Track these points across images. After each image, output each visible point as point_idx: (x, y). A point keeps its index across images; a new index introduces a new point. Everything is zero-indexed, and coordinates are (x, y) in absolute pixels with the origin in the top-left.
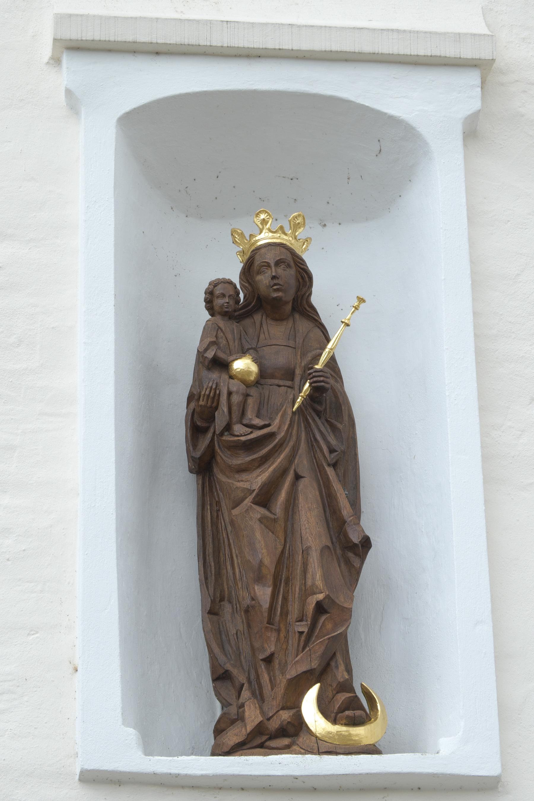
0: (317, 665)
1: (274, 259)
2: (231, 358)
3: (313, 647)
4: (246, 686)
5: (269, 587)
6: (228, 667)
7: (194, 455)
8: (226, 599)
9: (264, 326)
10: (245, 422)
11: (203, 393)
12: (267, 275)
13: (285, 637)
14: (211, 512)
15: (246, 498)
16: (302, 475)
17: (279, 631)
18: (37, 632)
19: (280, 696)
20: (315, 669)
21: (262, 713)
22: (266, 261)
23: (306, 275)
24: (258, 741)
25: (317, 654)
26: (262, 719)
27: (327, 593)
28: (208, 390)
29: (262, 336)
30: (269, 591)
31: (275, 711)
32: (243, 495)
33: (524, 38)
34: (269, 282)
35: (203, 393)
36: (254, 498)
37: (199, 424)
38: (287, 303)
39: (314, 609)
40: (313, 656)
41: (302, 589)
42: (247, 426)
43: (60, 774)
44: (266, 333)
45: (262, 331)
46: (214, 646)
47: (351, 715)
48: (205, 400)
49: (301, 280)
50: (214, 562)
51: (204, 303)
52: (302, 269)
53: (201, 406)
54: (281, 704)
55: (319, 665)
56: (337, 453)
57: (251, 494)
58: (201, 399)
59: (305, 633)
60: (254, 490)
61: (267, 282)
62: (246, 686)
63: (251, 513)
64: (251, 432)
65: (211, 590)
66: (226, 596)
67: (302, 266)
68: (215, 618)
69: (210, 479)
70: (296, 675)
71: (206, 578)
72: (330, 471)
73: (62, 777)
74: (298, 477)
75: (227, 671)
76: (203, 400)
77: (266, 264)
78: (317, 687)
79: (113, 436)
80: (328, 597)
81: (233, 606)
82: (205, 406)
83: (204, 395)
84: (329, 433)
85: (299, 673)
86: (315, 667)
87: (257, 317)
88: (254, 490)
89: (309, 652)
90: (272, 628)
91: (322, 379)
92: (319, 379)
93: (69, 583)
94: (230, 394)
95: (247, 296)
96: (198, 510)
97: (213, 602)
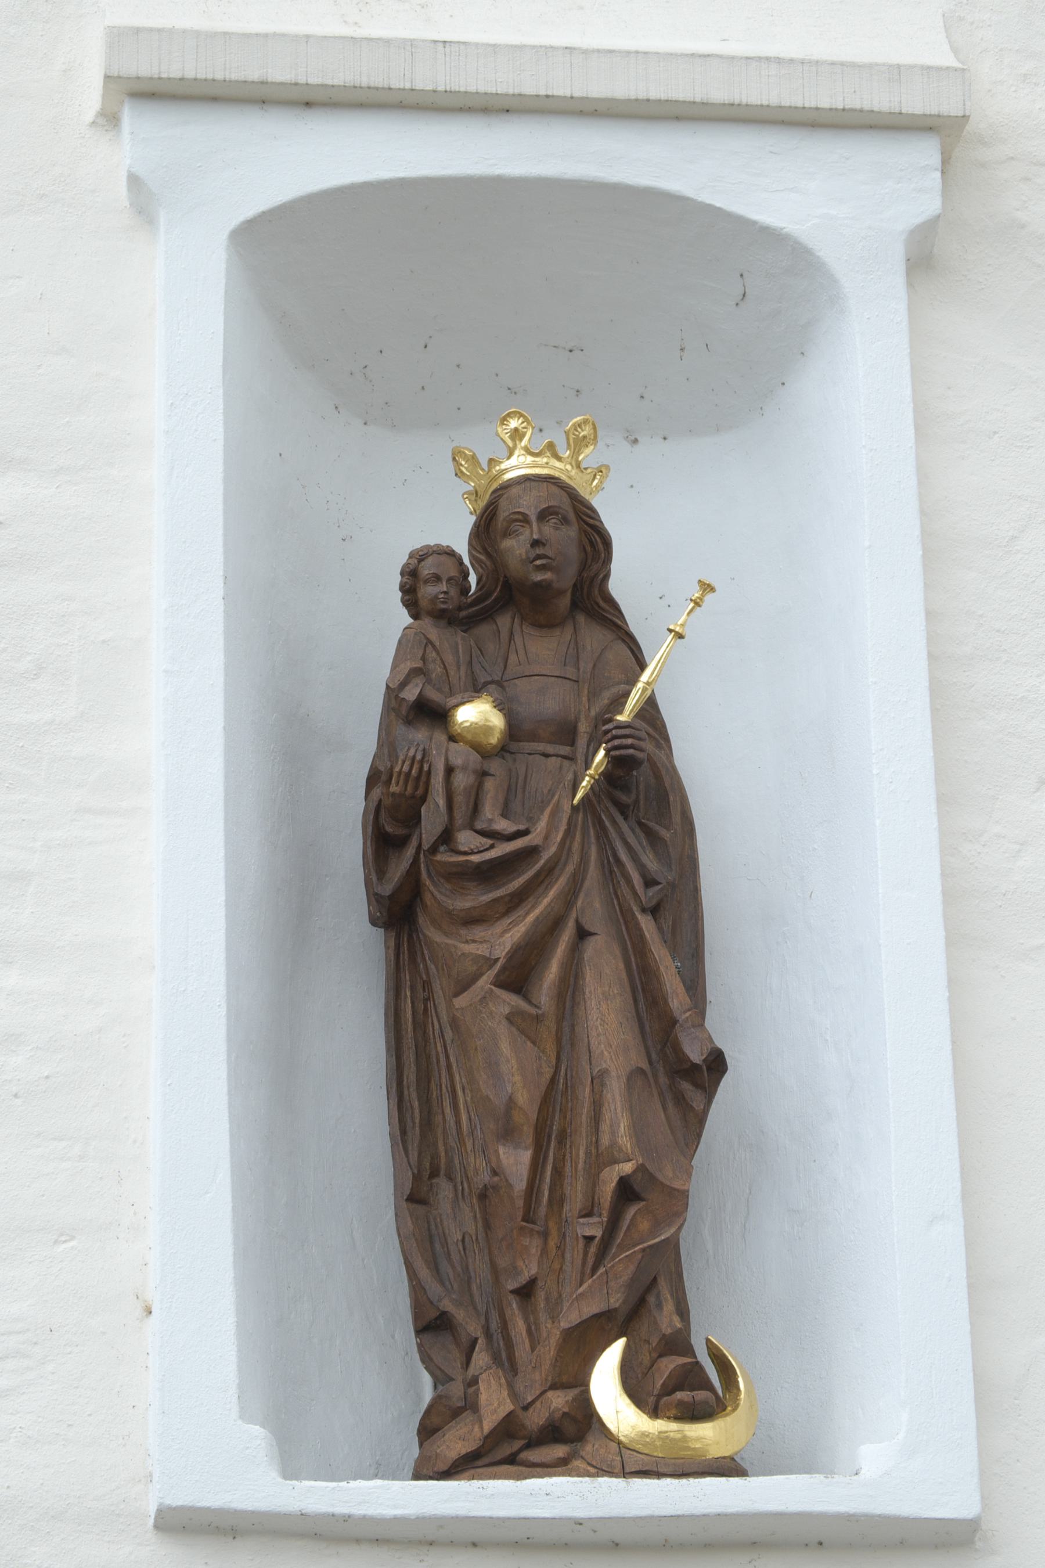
0: (620, 1301)
1: (536, 508)
2: (452, 701)
3: (613, 1266)
4: (481, 1343)
5: (526, 1148)
6: (447, 1305)
7: (379, 890)
8: (442, 1172)
9: (517, 638)
10: (479, 826)
11: (397, 769)
12: (522, 537)
13: (558, 1248)
14: (413, 1003)
15: (482, 974)
16: (592, 930)
17: (545, 1235)
18: (73, 1238)
19: (548, 1362)
20: (615, 1310)
21: (514, 1395)
22: (521, 510)
23: (598, 539)
24: (506, 1450)
25: (621, 1281)
26: (512, 1407)
27: (641, 1161)
28: (408, 763)
29: (513, 658)
30: (526, 1156)
31: (538, 1392)
33: (1025, 75)
34: (527, 553)
35: (397, 769)
36: (497, 975)
37: (389, 829)
38: (561, 593)
40: (612, 1284)
41: (591, 1153)
42: (483, 833)
44: (521, 652)
45: (513, 647)
46: (420, 1265)
47: (686, 1399)
48: (401, 782)
49: (588, 548)
50: (419, 1100)
51: (400, 594)
52: (592, 527)
53: (393, 794)
55: (624, 1302)
56: (660, 887)
57: (491, 967)
59: (597, 1239)
60: (497, 960)
61: (523, 551)
62: (481, 1343)
63: (491, 1004)
64: (492, 847)
65: (414, 1155)
66: (443, 1166)
67: (591, 521)
68: (421, 1209)
69: (410, 937)
71: (403, 1132)
72: (646, 923)
74: (582, 934)
76: (397, 783)
77: (520, 517)
78: (620, 1344)
79: (222, 853)
80: (641, 1169)
81: (455, 1186)
82: (401, 795)
83: (400, 773)
84: (643, 848)
85: (585, 1317)
86: (617, 1305)
87: (504, 621)
88: (497, 960)
89: (605, 1277)
90: (532, 1230)
91: (630, 741)
93: (135, 1142)
94: (449, 770)
95: (484, 579)
96: (387, 998)
97: (417, 1178)
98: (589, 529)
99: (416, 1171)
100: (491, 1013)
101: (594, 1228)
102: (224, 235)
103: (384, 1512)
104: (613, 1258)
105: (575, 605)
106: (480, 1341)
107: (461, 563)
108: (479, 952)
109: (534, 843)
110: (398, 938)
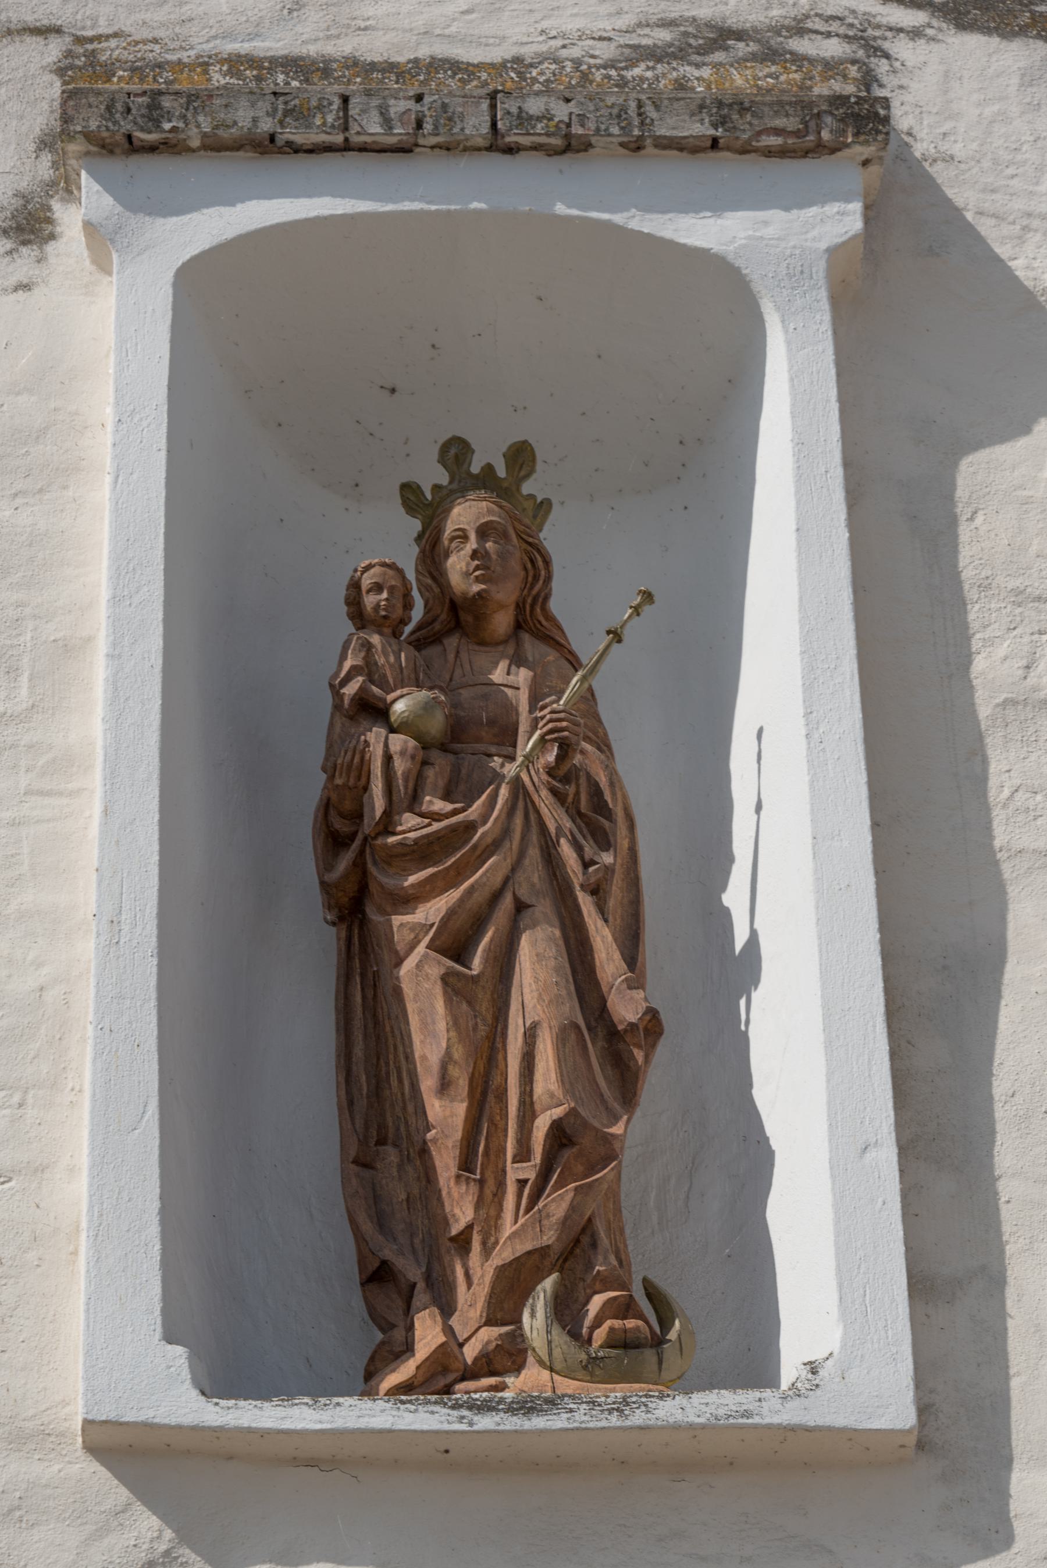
0: (554, 1238)
1: (475, 523)
2: (390, 697)
3: (545, 1205)
4: (421, 1286)
5: (462, 1101)
6: (387, 1253)
7: (326, 878)
8: (390, 1141)
9: (464, 656)
10: (417, 810)
11: (339, 761)
12: (462, 553)
13: (495, 1195)
14: (363, 989)
15: (419, 942)
16: (528, 902)
17: (481, 1182)
18: (10, 1180)
19: (483, 1299)
20: (548, 1247)
21: (448, 1330)
22: (461, 526)
23: (538, 556)
24: (442, 1382)
25: (554, 1219)
26: (444, 1339)
27: (573, 1105)
28: (349, 754)
29: (458, 672)
30: (461, 1108)
31: (473, 1329)
32: (412, 936)
33: (944, 134)
34: (468, 564)
35: (339, 761)
36: (432, 940)
37: (337, 826)
38: (502, 606)
39: (547, 1135)
40: (545, 1222)
41: (524, 1102)
42: (422, 815)
43: (49, 1434)
44: (467, 666)
45: (458, 663)
46: (362, 1218)
47: (617, 1326)
48: (344, 775)
49: (529, 566)
50: (366, 1074)
51: (346, 608)
52: (530, 544)
53: (337, 786)
54: (484, 1315)
55: (558, 1240)
56: (597, 866)
57: (427, 933)
58: (337, 774)
59: (530, 1182)
60: (432, 925)
61: (463, 565)
62: (421, 1286)
63: (426, 967)
64: (429, 825)
65: (359, 1123)
66: (390, 1135)
67: (531, 540)
68: (367, 1173)
69: (361, 927)
70: (512, 1258)
71: (351, 1103)
72: (586, 903)
73: (51, 1439)
74: (520, 907)
75: (384, 1263)
76: (341, 774)
77: (460, 533)
78: (554, 1276)
79: (157, 817)
80: (572, 1113)
81: (400, 1151)
82: (345, 785)
83: (343, 765)
84: (584, 837)
85: (518, 1255)
86: (550, 1242)
87: (452, 642)
88: (432, 925)
89: (537, 1216)
90: (468, 1178)
91: (564, 724)
92: (558, 724)
93: (72, 1090)
94: (388, 758)
95: (431, 602)
96: (337, 984)
97: (363, 1142)
98: (529, 548)
99: (361, 1138)
100: (427, 975)
101: (529, 1171)
102: (170, 276)
103: (308, 1427)
104: (549, 1196)
105: (519, 626)
106: (418, 1286)
107: (404, 578)
108: (416, 921)
109: (472, 818)
110: (350, 930)
